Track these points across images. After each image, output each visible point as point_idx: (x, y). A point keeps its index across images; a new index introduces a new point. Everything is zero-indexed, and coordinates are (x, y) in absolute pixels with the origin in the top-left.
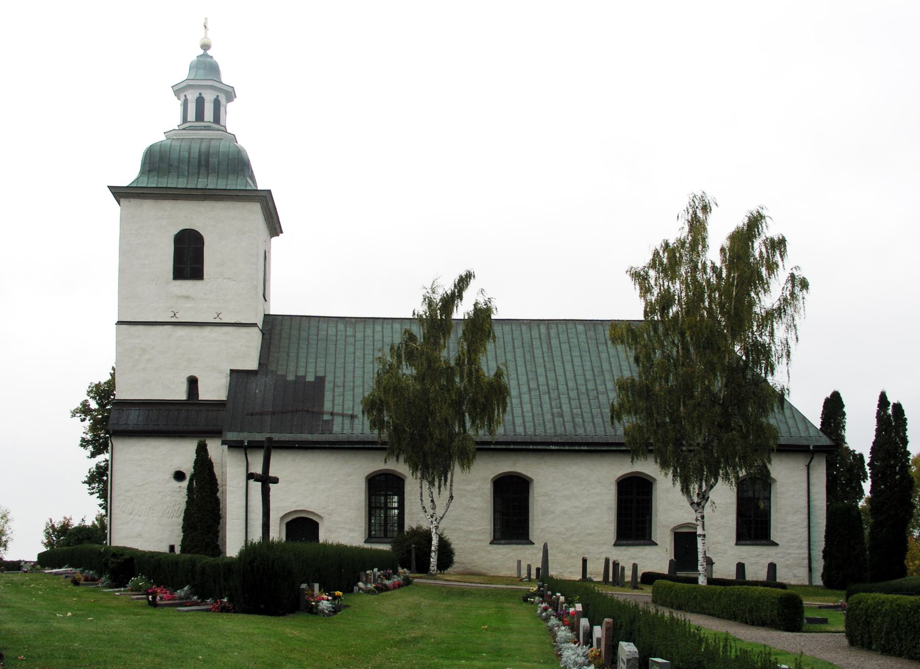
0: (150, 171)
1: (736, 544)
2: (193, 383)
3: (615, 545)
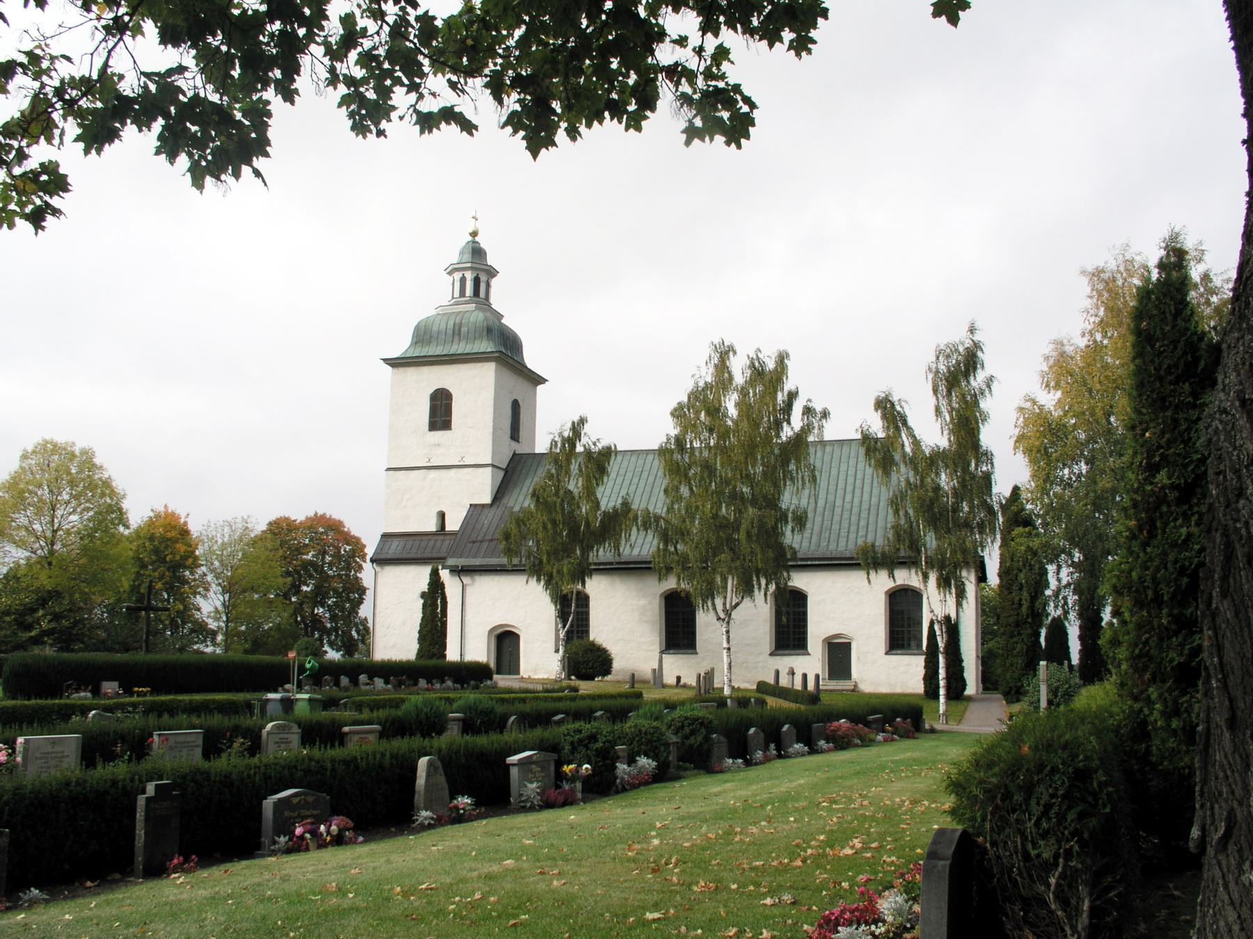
1: (886, 653)
2: (442, 516)
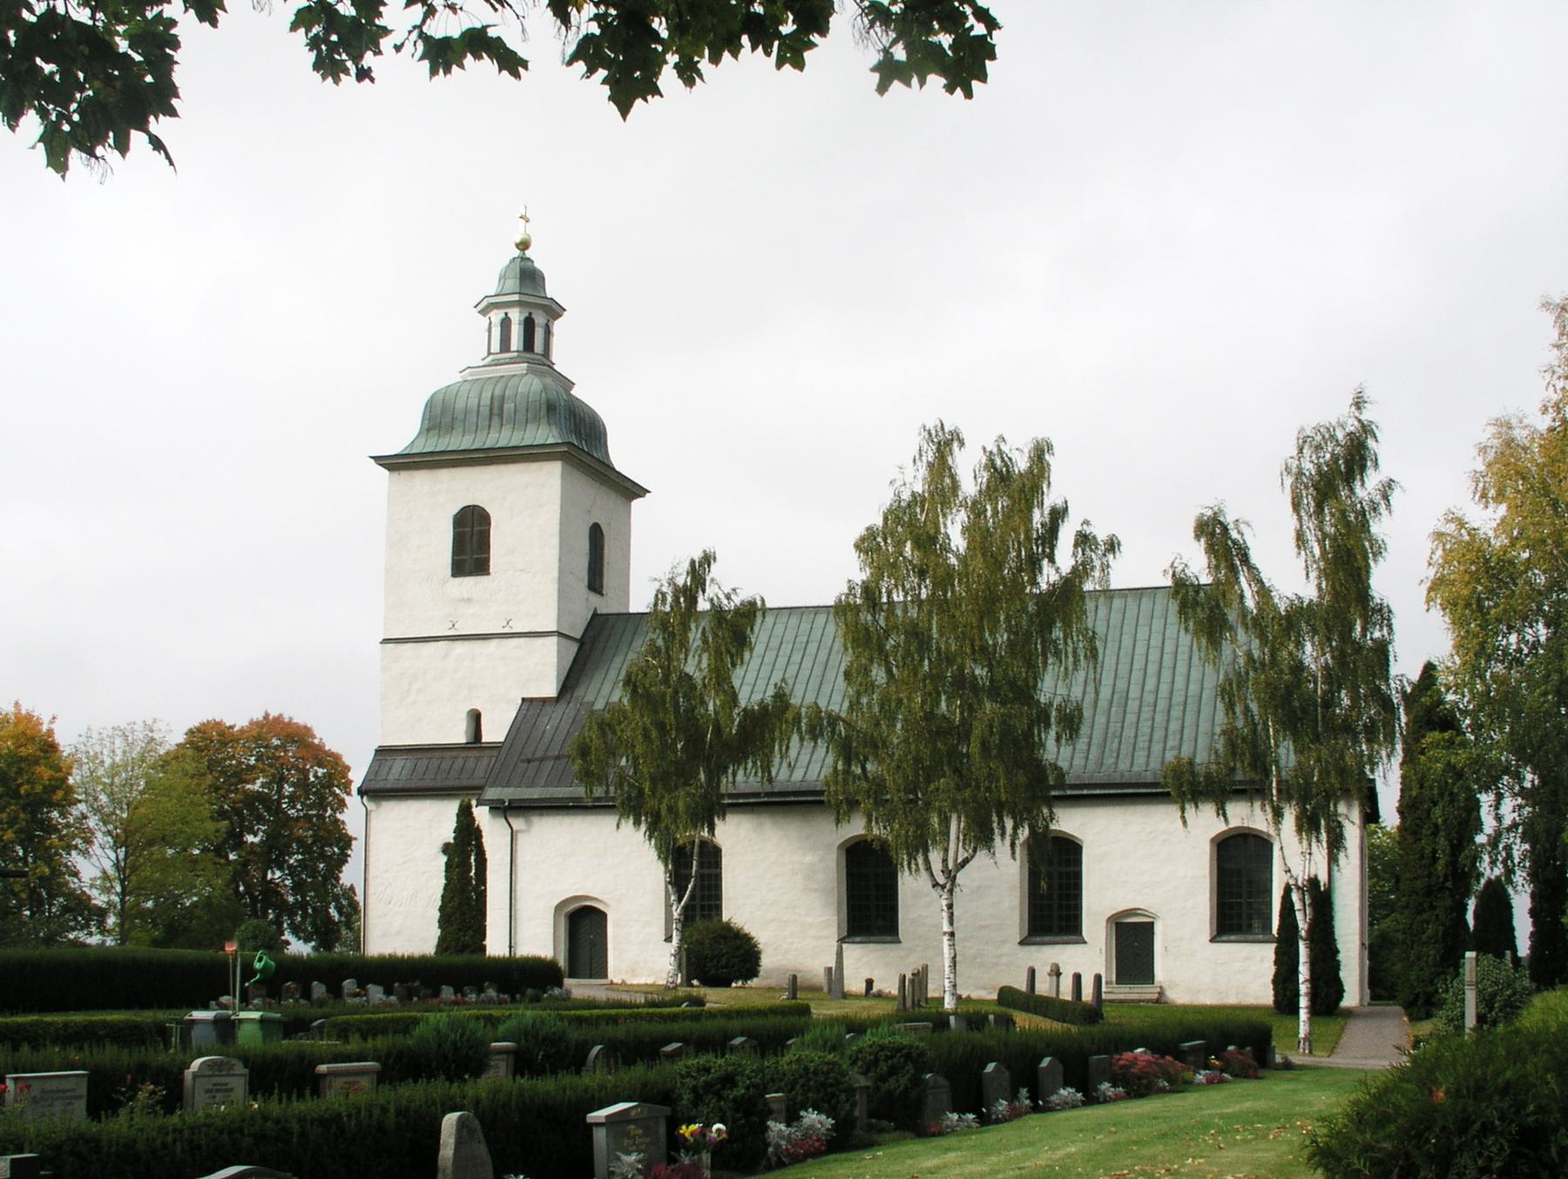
0: (428, 430)
2: (476, 718)
3: (1022, 943)
